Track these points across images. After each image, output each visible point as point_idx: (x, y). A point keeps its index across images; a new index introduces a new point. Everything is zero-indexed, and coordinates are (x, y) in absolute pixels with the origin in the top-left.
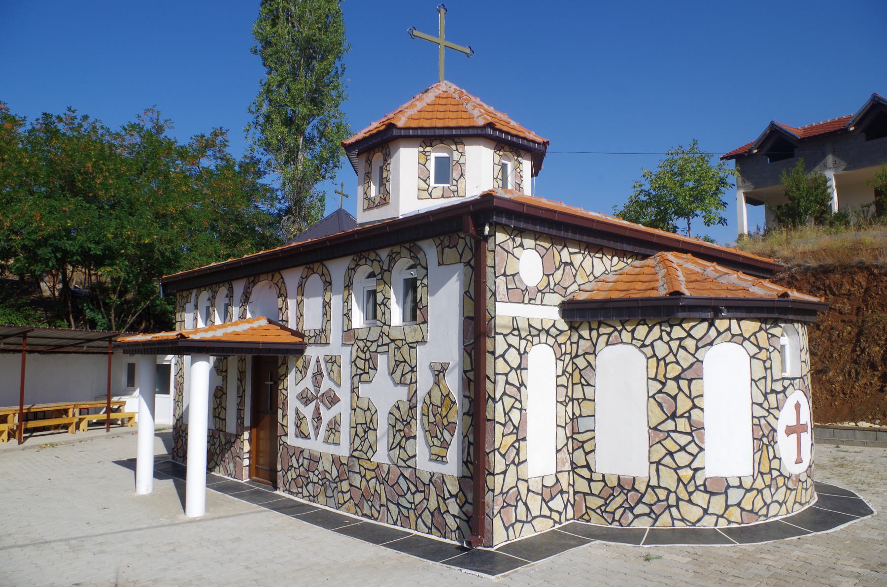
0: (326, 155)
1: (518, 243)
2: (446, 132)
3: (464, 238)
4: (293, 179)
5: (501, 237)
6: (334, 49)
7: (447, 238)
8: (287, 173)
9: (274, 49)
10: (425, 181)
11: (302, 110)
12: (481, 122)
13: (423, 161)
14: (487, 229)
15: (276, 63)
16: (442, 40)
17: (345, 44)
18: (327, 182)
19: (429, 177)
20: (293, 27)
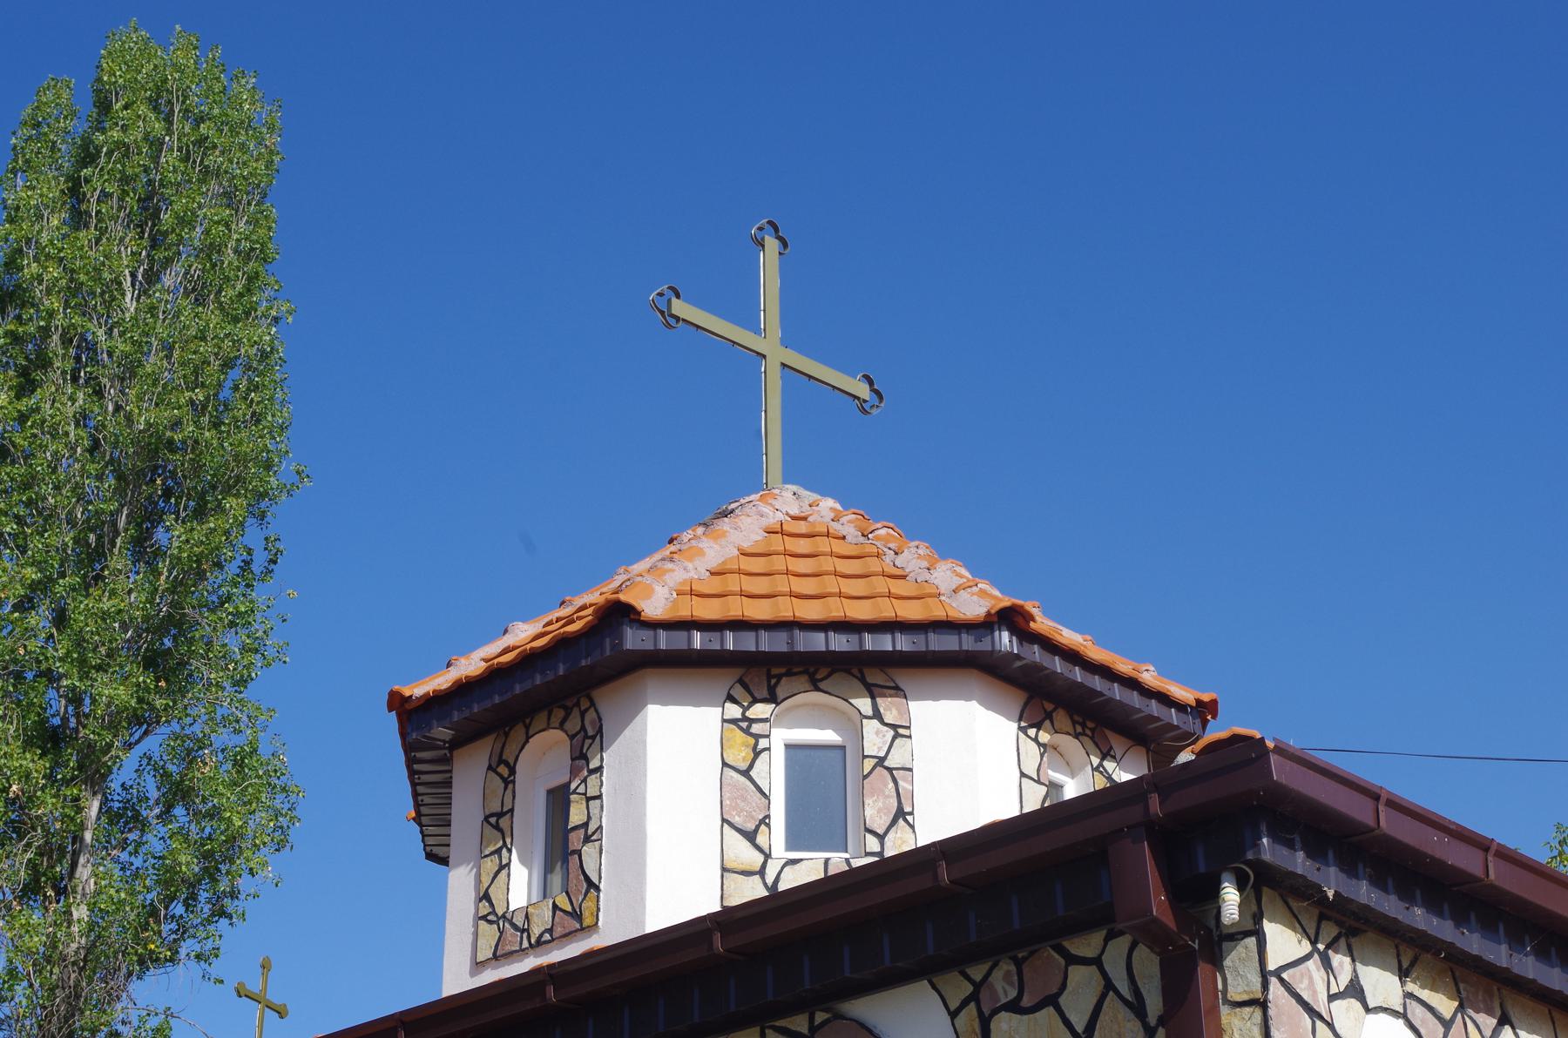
0: (188, 863)
1: (1344, 980)
2: (840, 643)
3: (1097, 962)
4: (51, 955)
5: (1283, 942)
6: (243, 481)
7: (1006, 966)
8: (28, 928)
9: (19, 470)
10: (751, 837)
11: (112, 691)
12: (972, 606)
13: (739, 757)
14: (1231, 896)
15: (19, 520)
16: (770, 343)
17: (287, 468)
18: (185, 973)
19: (765, 821)
20: (99, 393)
